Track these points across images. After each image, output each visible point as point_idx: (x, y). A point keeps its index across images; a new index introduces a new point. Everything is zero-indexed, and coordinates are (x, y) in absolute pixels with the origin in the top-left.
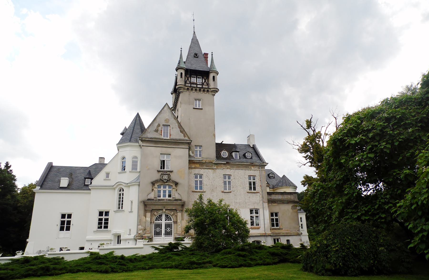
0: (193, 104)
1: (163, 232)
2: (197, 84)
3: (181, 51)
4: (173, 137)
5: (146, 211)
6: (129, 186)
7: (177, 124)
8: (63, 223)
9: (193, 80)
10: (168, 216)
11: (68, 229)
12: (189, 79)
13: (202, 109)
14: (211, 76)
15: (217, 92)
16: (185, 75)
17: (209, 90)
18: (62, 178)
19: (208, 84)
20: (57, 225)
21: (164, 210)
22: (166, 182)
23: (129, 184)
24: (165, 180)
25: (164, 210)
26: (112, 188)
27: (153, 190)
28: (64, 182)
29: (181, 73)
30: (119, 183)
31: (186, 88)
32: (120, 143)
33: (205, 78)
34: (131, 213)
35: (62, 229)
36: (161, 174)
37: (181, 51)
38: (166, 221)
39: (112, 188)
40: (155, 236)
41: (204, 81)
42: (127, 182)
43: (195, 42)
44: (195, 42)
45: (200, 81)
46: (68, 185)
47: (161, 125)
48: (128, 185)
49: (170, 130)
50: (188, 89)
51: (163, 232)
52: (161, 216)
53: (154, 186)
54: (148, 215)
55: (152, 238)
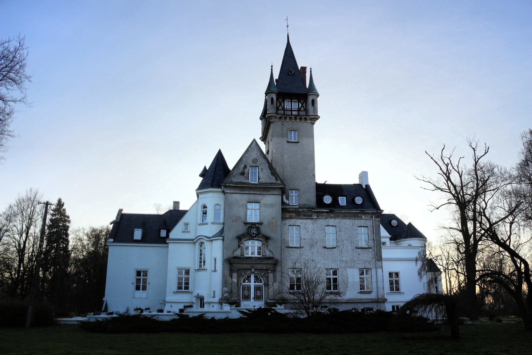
0: (287, 137)
1: (252, 295)
2: (292, 111)
3: (272, 69)
4: (263, 180)
5: (231, 271)
6: (212, 241)
7: (267, 165)
8: (138, 280)
9: (287, 105)
10: (257, 277)
11: (144, 288)
12: (282, 104)
13: (298, 142)
14: (310, 98)
15: (317, 119)
16: (277, 99)
17: (308, 117)
18: (135, 229)
19: (306, 110)
20: (133, 284)
21: (253, 270)
22: (255, 237)
23: (212, 239)
24: (254, 234)
25: (253, 270)
26: (192, 241)
27: (239, 246)
28: (138, 234)
29: (272, 99)
30: (199, 238)
31: (278, 116)
32: (202, 186)
33: (302, 101)
34: (215, 273)
35: (138, 288)
36: (249, 227)
37: (272, 69)
38: (255, 282)
39: (192, 241)
40: (242, 301)
41: (300, 105)
42: (210, 236)
43: (289, 55)
44: (289, 55)
45: (295, 105)
46: (142, 237)
47: (248, 166)
48: (210, 239)
49: (258, 172)
50: (280, 118)
51: (252, 295)
52: (249, 277)
53: (241, 241)
54: (235, 275)
55: (240, 302)
